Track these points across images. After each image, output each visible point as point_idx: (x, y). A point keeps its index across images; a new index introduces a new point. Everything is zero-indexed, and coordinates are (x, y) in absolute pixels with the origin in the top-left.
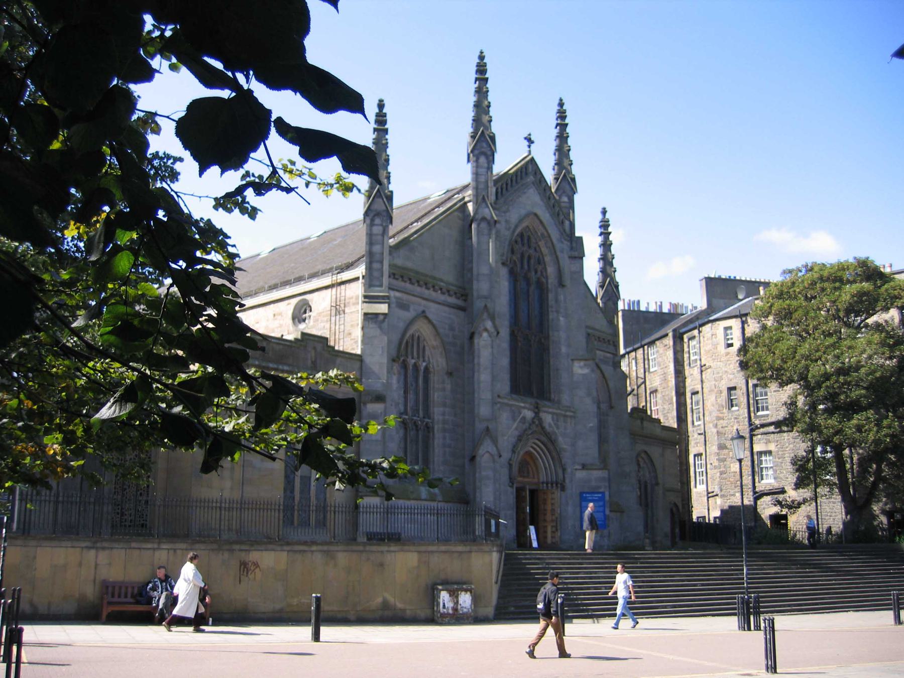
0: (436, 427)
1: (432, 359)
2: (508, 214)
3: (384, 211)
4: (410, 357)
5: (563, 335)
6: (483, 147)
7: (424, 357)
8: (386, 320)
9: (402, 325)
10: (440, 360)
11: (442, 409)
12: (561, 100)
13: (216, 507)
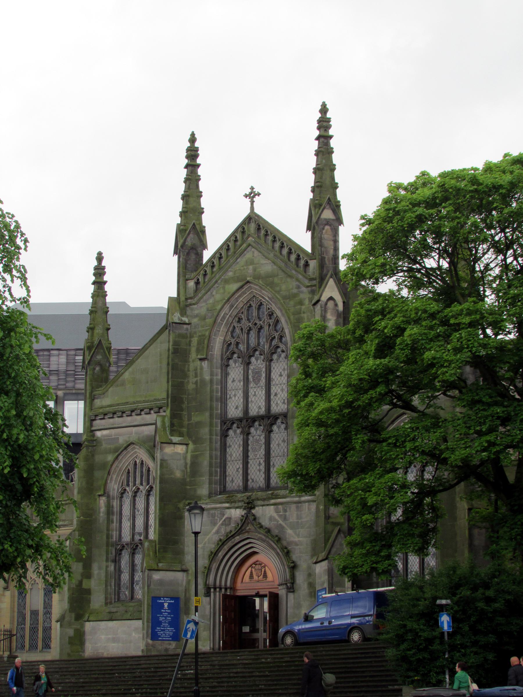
12: (193, 135)
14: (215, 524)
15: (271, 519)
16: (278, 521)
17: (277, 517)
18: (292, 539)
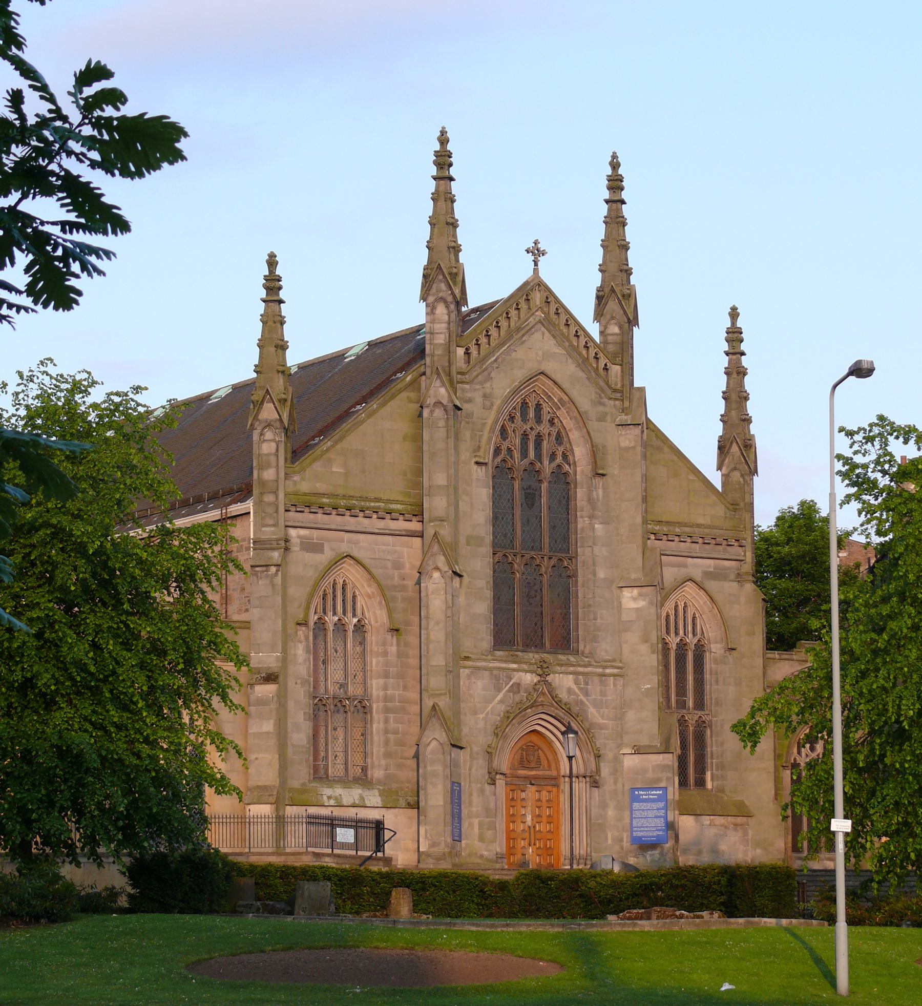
0: (375, 706)
1: (369, 611)
2: (488, 385)
3: (276, 420)
4: (330, 613)
5: (601, 551)
6: (439, 291)
7: (354, 610)
8: (280, 573)
9: (312, 574)
10: (378, 612)
11: (382, 681)
13: (268, 822)
14: (499, 690)
15: (570, 691)
16: (578, 696)
17: (577, 691)
18: (595, 720)
